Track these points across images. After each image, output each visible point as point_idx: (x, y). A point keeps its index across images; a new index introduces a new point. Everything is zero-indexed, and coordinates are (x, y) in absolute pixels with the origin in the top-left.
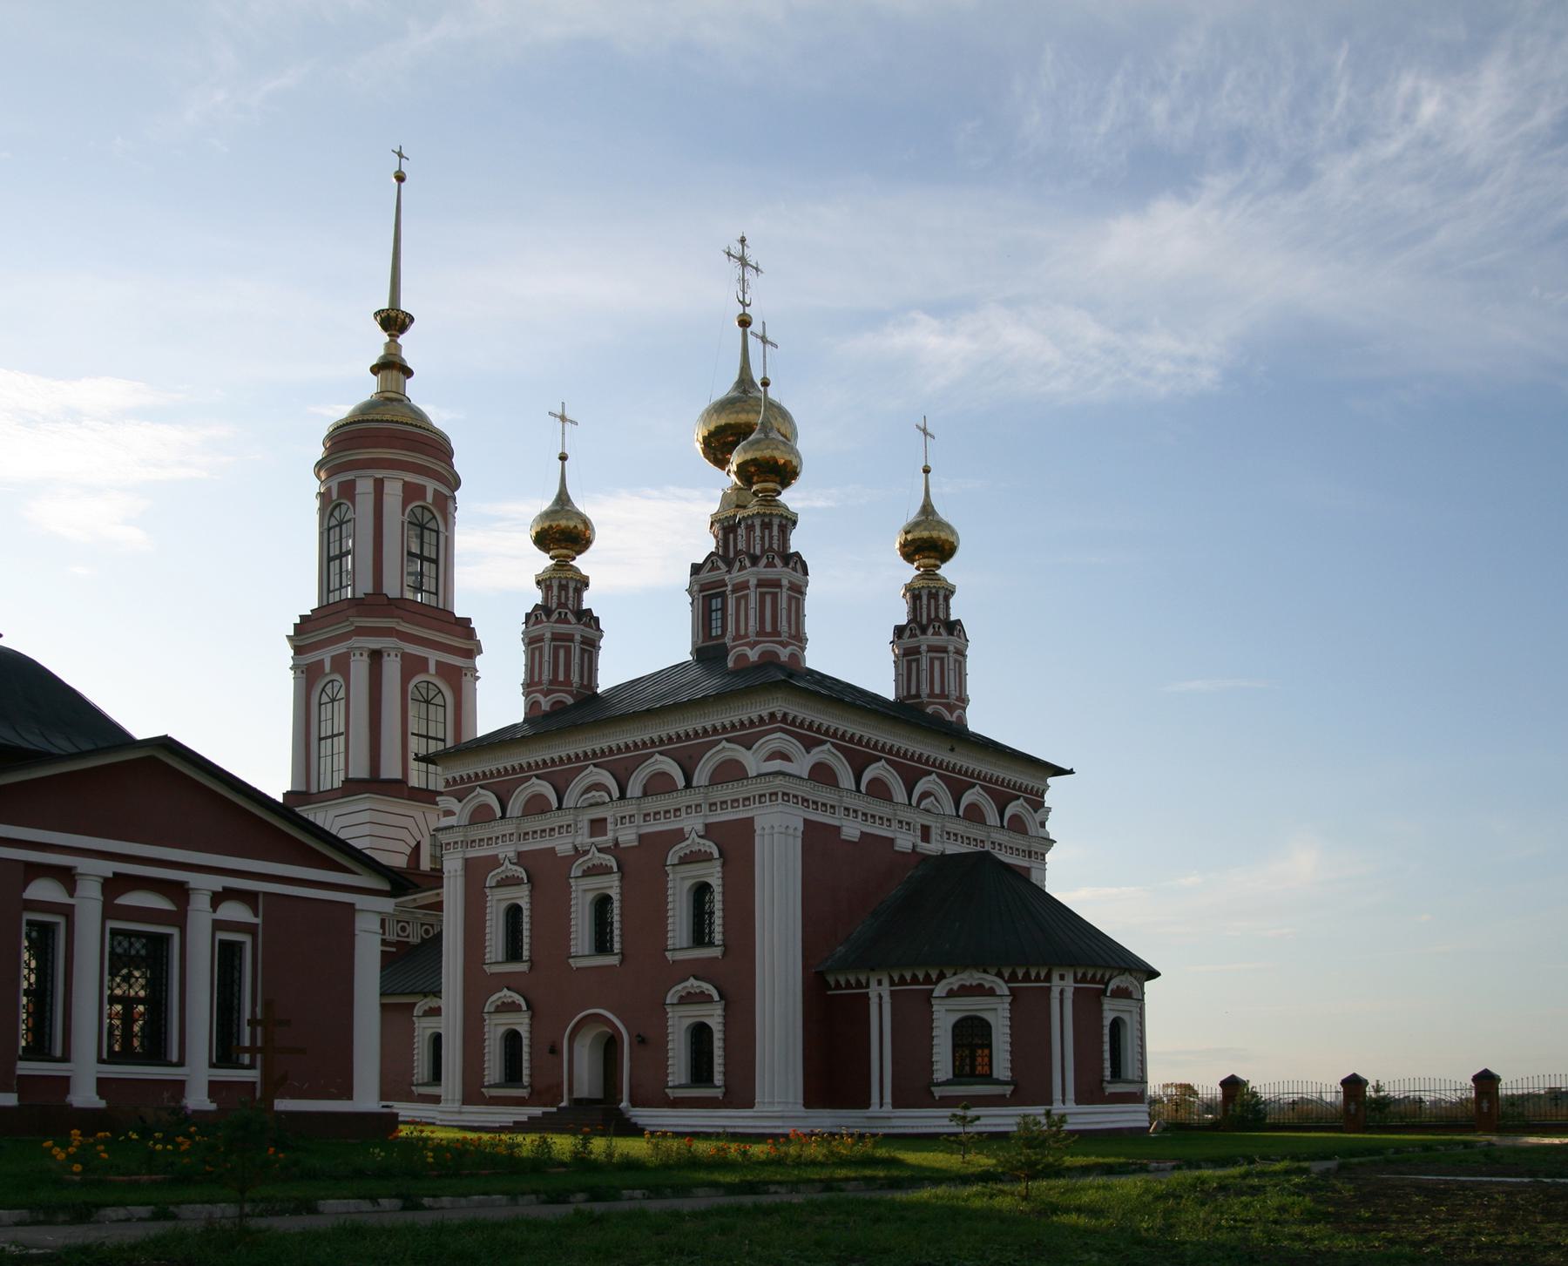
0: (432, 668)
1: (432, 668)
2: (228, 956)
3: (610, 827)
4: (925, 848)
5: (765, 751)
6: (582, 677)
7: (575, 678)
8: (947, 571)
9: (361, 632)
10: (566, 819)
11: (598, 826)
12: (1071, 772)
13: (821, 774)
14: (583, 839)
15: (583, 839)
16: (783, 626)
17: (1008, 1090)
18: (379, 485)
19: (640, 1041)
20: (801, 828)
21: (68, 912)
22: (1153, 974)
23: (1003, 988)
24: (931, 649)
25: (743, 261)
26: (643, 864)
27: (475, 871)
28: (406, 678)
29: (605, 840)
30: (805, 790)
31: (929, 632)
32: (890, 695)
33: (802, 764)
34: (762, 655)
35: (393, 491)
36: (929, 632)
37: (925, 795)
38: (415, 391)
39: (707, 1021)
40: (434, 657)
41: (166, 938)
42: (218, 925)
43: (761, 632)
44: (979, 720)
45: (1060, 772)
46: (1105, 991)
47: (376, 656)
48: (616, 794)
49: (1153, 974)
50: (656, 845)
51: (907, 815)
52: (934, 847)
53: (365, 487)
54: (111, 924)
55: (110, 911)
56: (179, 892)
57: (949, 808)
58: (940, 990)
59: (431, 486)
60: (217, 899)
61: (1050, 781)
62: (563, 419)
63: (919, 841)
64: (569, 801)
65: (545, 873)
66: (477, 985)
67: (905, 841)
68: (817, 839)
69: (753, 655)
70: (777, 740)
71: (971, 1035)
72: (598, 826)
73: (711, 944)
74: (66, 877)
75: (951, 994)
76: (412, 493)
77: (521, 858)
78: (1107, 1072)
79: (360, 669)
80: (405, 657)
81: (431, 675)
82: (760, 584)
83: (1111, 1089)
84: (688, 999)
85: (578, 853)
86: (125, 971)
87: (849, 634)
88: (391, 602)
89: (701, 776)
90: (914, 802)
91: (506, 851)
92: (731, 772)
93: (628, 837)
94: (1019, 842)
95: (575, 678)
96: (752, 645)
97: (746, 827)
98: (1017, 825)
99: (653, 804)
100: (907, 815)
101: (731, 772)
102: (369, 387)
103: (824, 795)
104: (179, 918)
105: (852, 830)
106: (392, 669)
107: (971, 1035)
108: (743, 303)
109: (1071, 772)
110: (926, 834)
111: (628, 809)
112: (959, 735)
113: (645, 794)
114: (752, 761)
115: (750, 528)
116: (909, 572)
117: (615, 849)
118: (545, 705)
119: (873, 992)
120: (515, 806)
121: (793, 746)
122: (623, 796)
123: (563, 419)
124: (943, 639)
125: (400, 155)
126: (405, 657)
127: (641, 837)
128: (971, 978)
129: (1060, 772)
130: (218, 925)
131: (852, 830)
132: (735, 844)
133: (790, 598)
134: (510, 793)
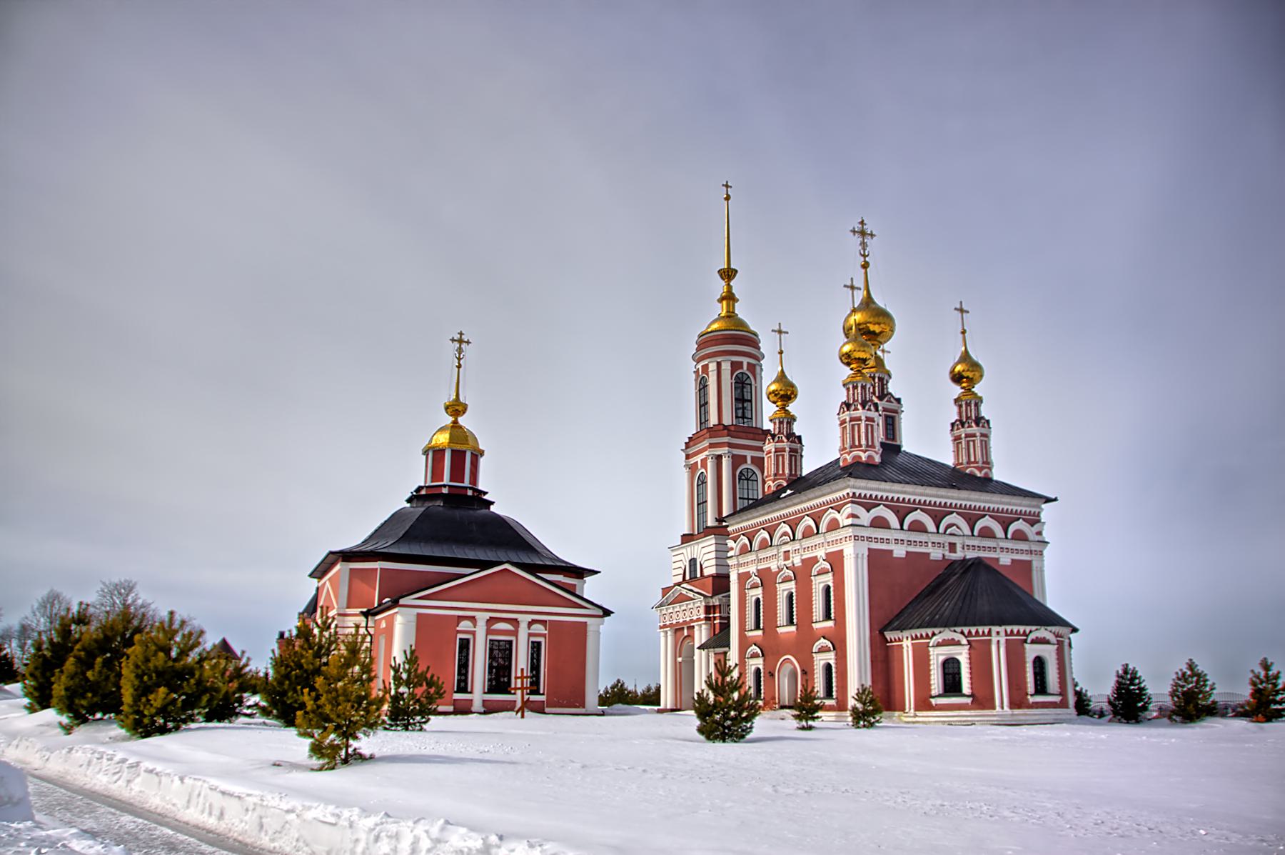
0: (749, 461)
1: (749, 461)
2: (536, 647)
4: (954, 556)
6: (790, 470)
7: (787, 471)
8: (792, 408)
9: (712, 446)
11: (787, 558)
12: (1055, 500)
14: (782, 563)
15: (782, 563)
16: (863, 442)
17: (969, 700)
18: (719, 364)
19: (804, 672)
20: (866, 553)
21: (474, 633)
24: (967, 436)
26: (802, 574)
27: (743, 578)
28: (734, 468)
31: (970, 419)
32: (949, 461)
33: (866, 517)
34: (854, 457)
35: (726, 367)
36: (970, 419)
38: (741, 311)
39: (958, 657)
41: (510, 642)
42: (530, 635)
43: (853, 446)
44: (997, 475)
45: (1048, 500)
46: (1025, 641)
47: (719, 458)
49: (1075, 630)
51: (937, 539)
52: (959, 555)
53: (712, 367)
54: (490, 637)
55: (489, 632)
56: (515, 622)
57: (967, 531)
58: (932, 642)
60: (531, 623)
61: (1043, 506)
62: (780, 332)
63: (947, 553)
64: (775, 542)
65: (767, 580)
66: (744, 644)
67: (936, 554)
68: (878, 562)
71: (950, 668)
72: (787, 558)
74: (473, 619)
75: (939, 645)
78: (1031, 687)
80: (734, 457)
81: (749, 464)
83: (1031, 699)
84: (823, 650)
86: (144, 699)
87: (927, 435)
88: (726, 427)
90: (941, 530)
91: (752, 569)
92: (834, 525)
96: (849, 453)
97: (840, 554)
99: (763, 555)
100: (937, 539)
101: (834, 525)
102: (721, 309)
104: (515, 633)
105: (899, 552)
106: (726, 463)
107: (950, 668)
108: (864, 256)
109: (1055, 500)
110: (952, 547)
111: (796, 546)
112: (985, 484)
114: (842, 518)
116: (957, 390)
119: (994, 639)
121: (860, 511)
123: (780, 332)
125: (727, 186)
126: (734, 457)
127: (803, 561)
128: (947, 634)
129: (1048, 500)
130: (530, 635)
131: (899, 552)
132: (836, 561)
133: (791, 456)
134: (820, 518)
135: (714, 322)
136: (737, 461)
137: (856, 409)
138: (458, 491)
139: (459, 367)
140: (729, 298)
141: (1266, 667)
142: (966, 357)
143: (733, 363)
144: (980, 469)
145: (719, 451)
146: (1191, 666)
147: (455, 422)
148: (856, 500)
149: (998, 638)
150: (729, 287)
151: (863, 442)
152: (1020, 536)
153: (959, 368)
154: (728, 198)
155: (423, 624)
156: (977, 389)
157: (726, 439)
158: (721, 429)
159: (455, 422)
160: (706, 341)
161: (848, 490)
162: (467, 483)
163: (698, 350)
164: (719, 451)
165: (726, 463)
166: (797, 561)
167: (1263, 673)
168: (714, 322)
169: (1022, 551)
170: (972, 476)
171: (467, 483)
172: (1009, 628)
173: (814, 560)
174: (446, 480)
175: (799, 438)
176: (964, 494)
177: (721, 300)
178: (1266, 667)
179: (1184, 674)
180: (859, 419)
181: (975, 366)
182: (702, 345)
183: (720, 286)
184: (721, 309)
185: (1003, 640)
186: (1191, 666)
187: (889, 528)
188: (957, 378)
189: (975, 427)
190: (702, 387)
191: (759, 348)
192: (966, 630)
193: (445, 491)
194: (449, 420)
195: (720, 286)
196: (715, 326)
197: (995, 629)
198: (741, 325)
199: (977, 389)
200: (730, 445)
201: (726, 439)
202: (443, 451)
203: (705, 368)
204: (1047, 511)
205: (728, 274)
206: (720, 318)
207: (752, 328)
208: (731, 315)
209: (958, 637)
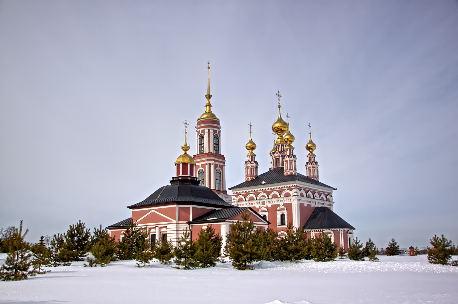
3: (266, 203)
5: (294, 191)
7: (255, 174)
8: (254, 152)
9: (208, 160)
10: (258, 201)
11: (263, 203)
13: (302, 195)
14: (261, 205)
15: (261, 205)
16: (293, 168)
18: (209, 130)
22: (355, 229)
23: (333, 233)
24: (313, 167)
25: (279, 95)
28: (215, 168)
29: (265, 206)
30: (299, 198)
31: (312, 162)
32: (306, 175)
33: (299, 193)
34: (291, 173)
35: (212, 131)
36: (312, 162)
37: (316, 196)
38: (213, 111)
40: (219, 164)
44: (320, 181)
45: (335, 189)
47: (210, 165)
48: (267, 198)
49: (355, 229)
50: (275, 207)
52: (316, 206)
53: (207, 131)
59: (217, 130)
62: (250, 125)
67: (313, 205)
68: (301, 206)
69: (289, 173)
70: (295, 190)
72: (263, 203)
73: (284, 224)
76: (215, 131)
77: (284, 205)
79: (207, 167)
81: (219, 168)
82: (290, 161)
85: (260, 208)
88: (212, 154)
89: (283, 195)
92: (288, 195)
93: (269, 205)
94: (329, 203)
95: (255, 174)
98: (328, 200)
102: (206, 110)
103: (302, 198)
106: (212, 167)
111: (269, 200)
112: (317, 183)
113: (272, 198)
114: (291, 193)
115: (287, 150)
116: (308, 152)
117: (267, 207)
118: (250, 179)
119: (341, 232)
120: (248, 198)
122: (268, 198)
123: (250, 125)
124: (315, 165)
129: (335, 189)
132: (289, 207)
133: (251, 169)
135: (204, 114)
136: (216, 166)
137: (291, 157)
138: (193, 179)
139: (186, 133)
140: (209, 105)
141: (393, 241)
142: (311, 142)
143: (214, 130)
144: (316, 178)
145: (210, 162)
146: (370, 241)
147: (186, 153)
148: (297, 187)
149: (342, 232)
150: (209, 101)
151: (289, 169)
152: (328, 200)
153: (309, 145)
154: (209, 68)
155: (233, 228)
156: (314, 152)
157: (213, 158)
158: (209, 154)
159: (186, 153)
160: (201, 122)
161: (295, 184)
162: (188, 175)
163: (198, 125)
164: (210, 162)
165: (212, 167)
166: (269, 205)
167: (392, 242)
168: (204, 114)
169: (328, 205)
170: (314, 180)
171: (188, 175)
172: (344, 229)
173: (279, 205)
174: (181, 175)
175: (223, 157)
176: (305, 184)
177: (206, 106)
178: (393, 241)
179: (396, 244)
180: (249, 167)
181: (314, 145)
182: (199, 123)
183: (206, 101)
184: (206, 110)
185: (343, 232)
186: (370, 241)
187: (310, 198)
188: (308, 148)
189: (315, 165)
190: (201, 138)
191: (219, 124)
192: (333, 229)
193: (180, 179)
194: (183, 152)
195: (206, 101)
196: (205, 116)
197: (341, 229)
198: (213, 116)
199: (314, 152)
200: (214, 160)
201: (213, 158)
202: (187, 164)
203: (203, 131)
204: (334, 193)
205: (209, 97)
206: (206, 113)
207: (217, 117)
208: (210, 112)
209: (330, 231)
